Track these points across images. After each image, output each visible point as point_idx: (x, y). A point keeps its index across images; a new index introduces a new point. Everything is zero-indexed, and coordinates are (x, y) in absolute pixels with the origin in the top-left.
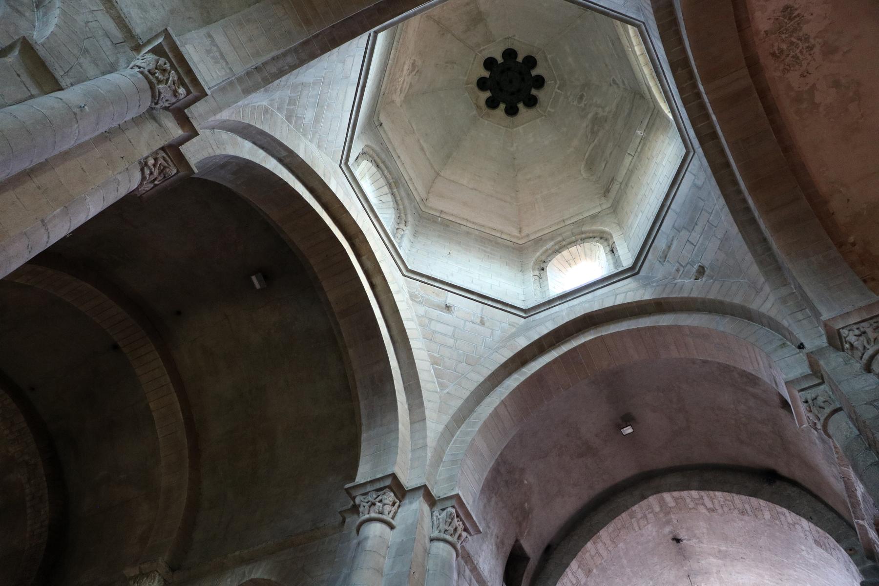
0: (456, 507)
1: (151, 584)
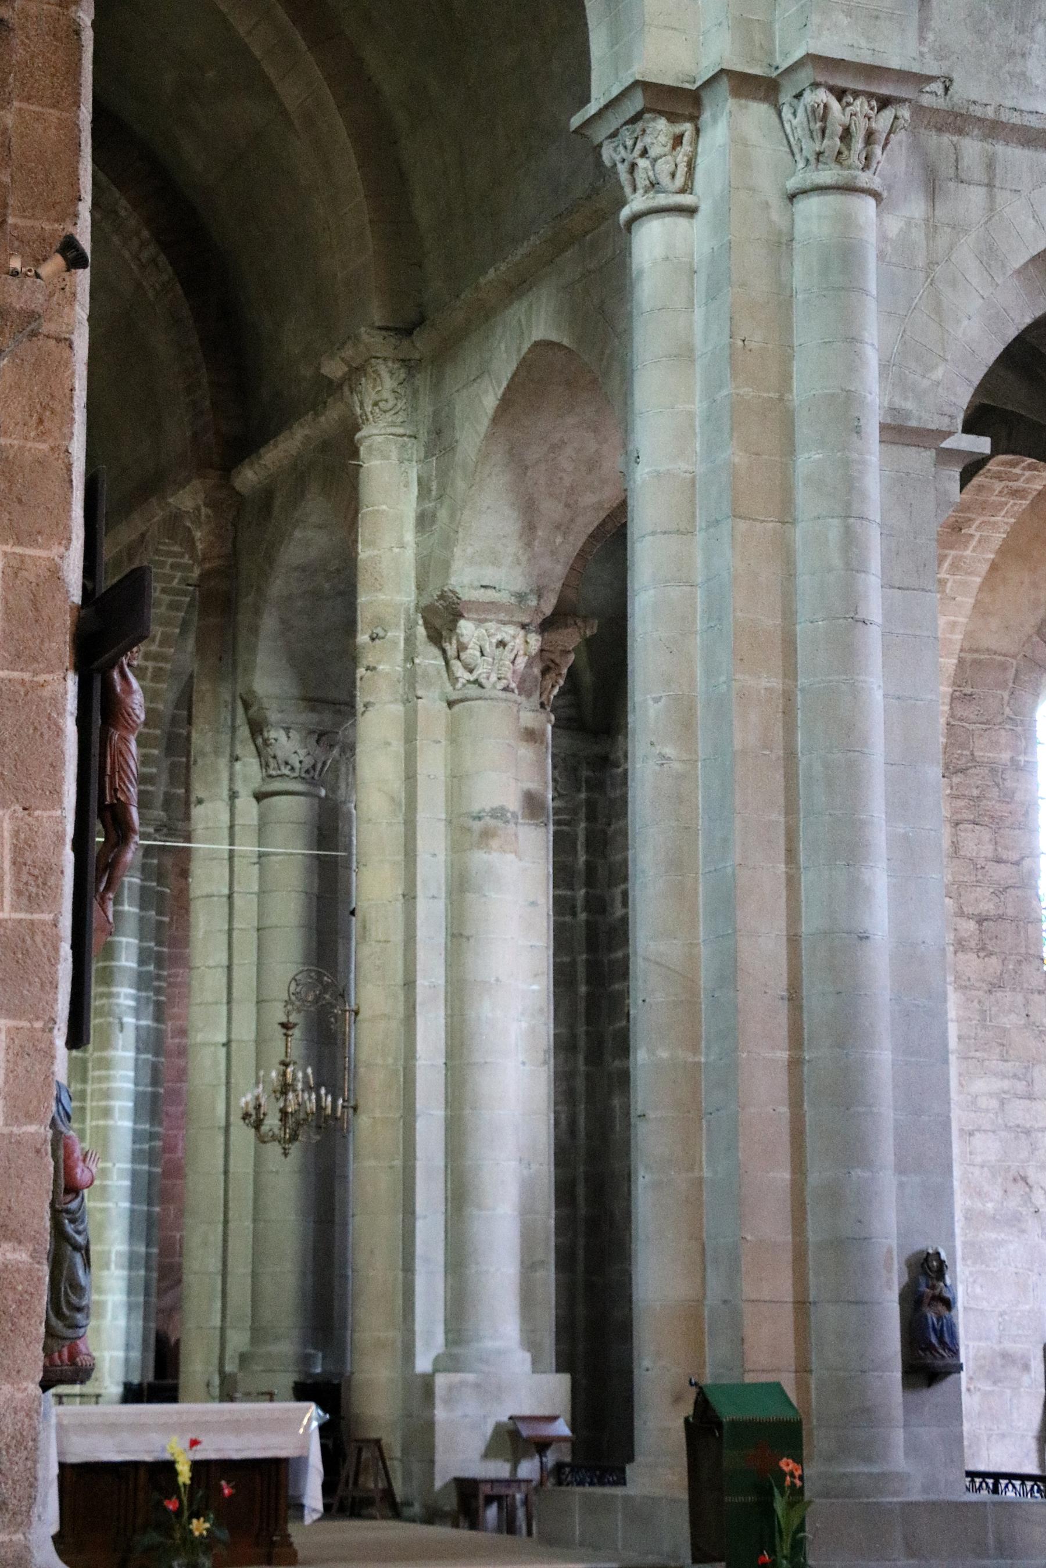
0: (819, 79)
1: (380, 388)
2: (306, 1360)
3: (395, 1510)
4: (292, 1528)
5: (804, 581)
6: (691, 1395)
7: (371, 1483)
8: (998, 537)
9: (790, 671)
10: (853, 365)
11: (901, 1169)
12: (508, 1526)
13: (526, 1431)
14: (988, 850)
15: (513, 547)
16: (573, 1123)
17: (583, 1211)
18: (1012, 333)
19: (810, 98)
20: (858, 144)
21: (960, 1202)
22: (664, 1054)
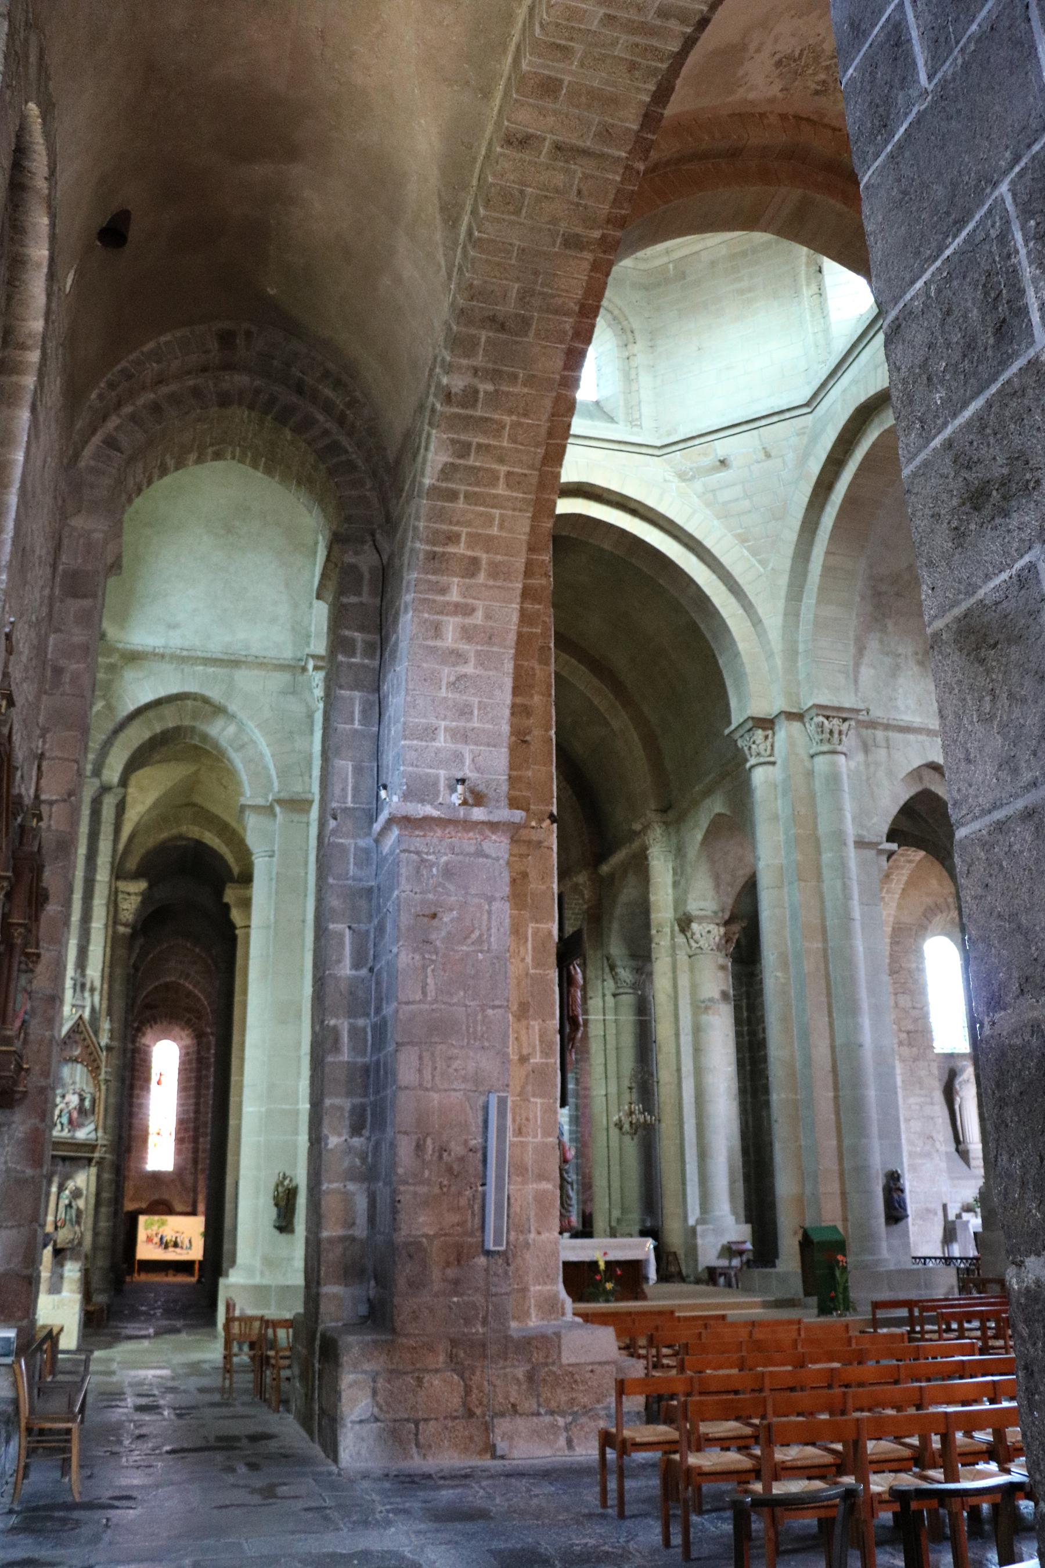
2: (643, 1221)
3: (683, 1279)
4: (645, 1286)
5: (829, 904)
6: (801, 1232)
7: (673, 1269)
8: (905, 878)
9: (825, 940)
10: (841, 820)
11: (881, 1137)
12: (729, 1285)
13: (734, 1247)
14: (909, 1004)
15: (711, 893)
16: (747, 1122)
17: (753, 1158)
18: (902, 803)
19: (816, 720)
20: (836, 735)
21: (905, 1148)
22: (783, 1096)
